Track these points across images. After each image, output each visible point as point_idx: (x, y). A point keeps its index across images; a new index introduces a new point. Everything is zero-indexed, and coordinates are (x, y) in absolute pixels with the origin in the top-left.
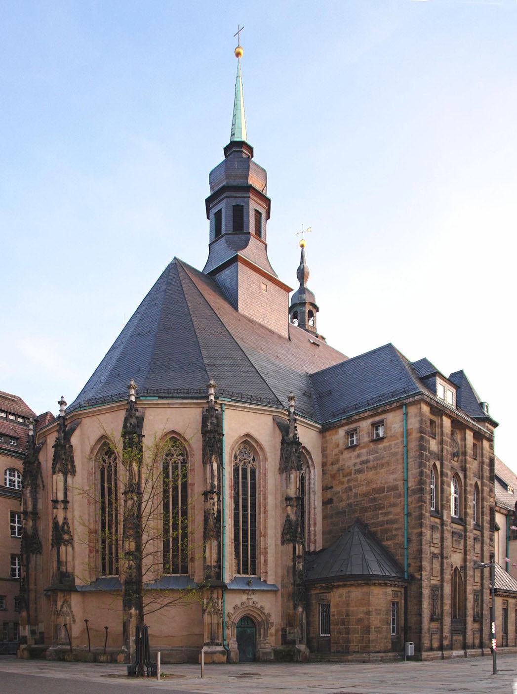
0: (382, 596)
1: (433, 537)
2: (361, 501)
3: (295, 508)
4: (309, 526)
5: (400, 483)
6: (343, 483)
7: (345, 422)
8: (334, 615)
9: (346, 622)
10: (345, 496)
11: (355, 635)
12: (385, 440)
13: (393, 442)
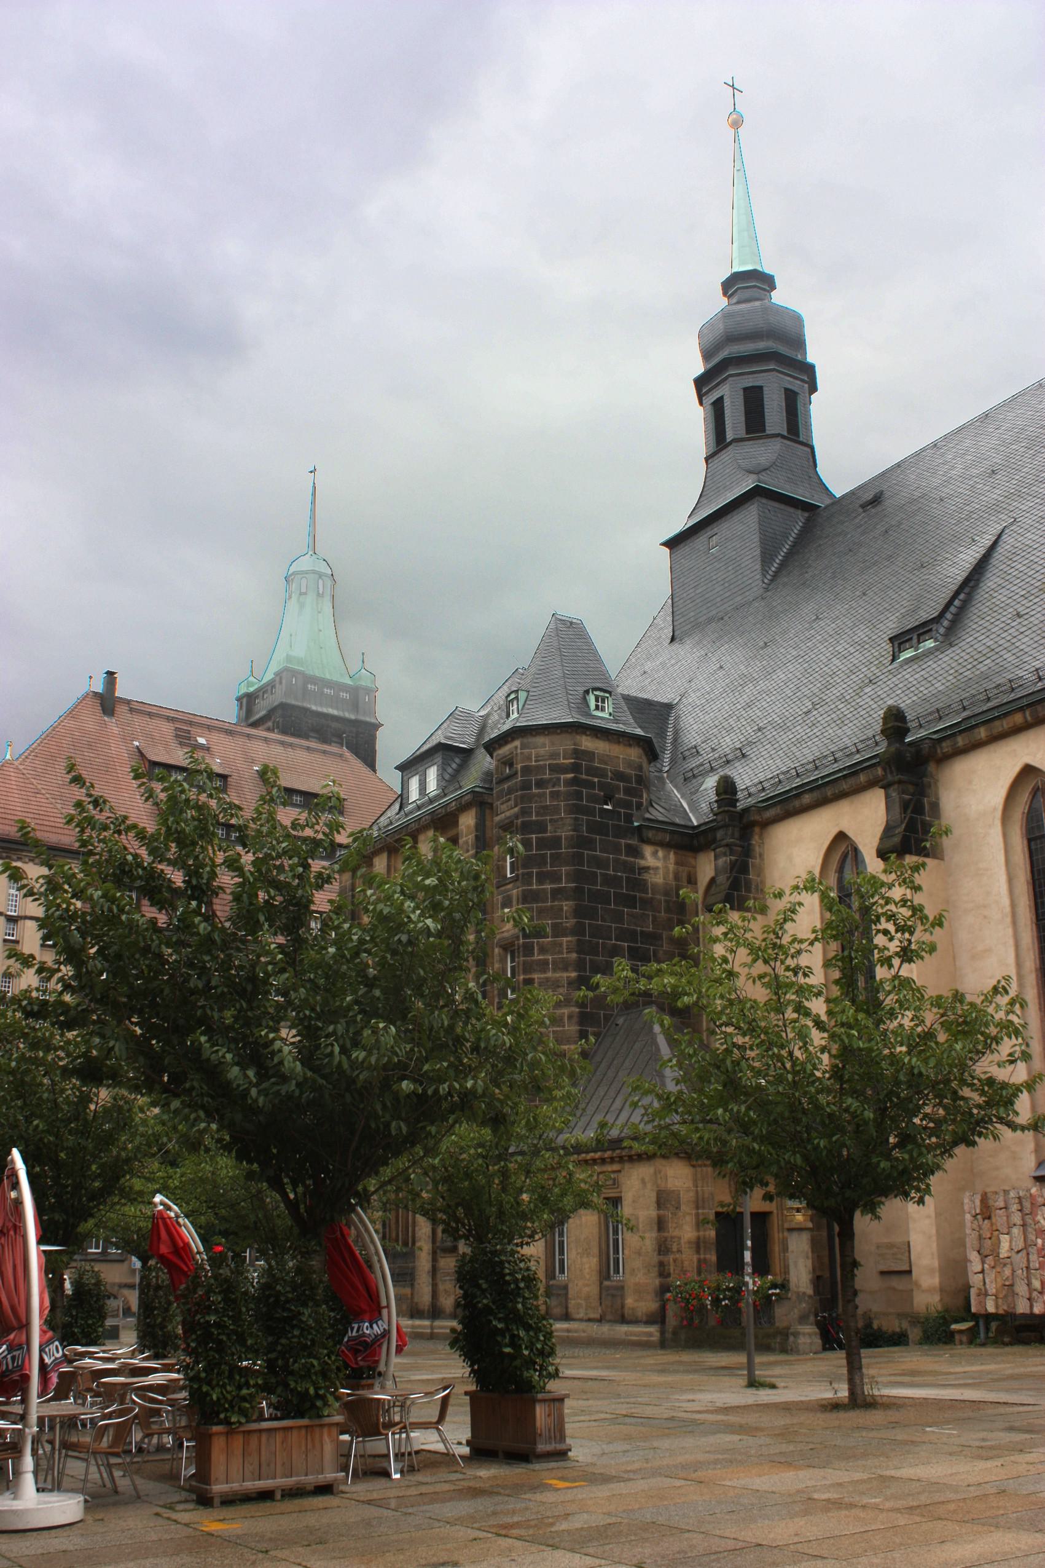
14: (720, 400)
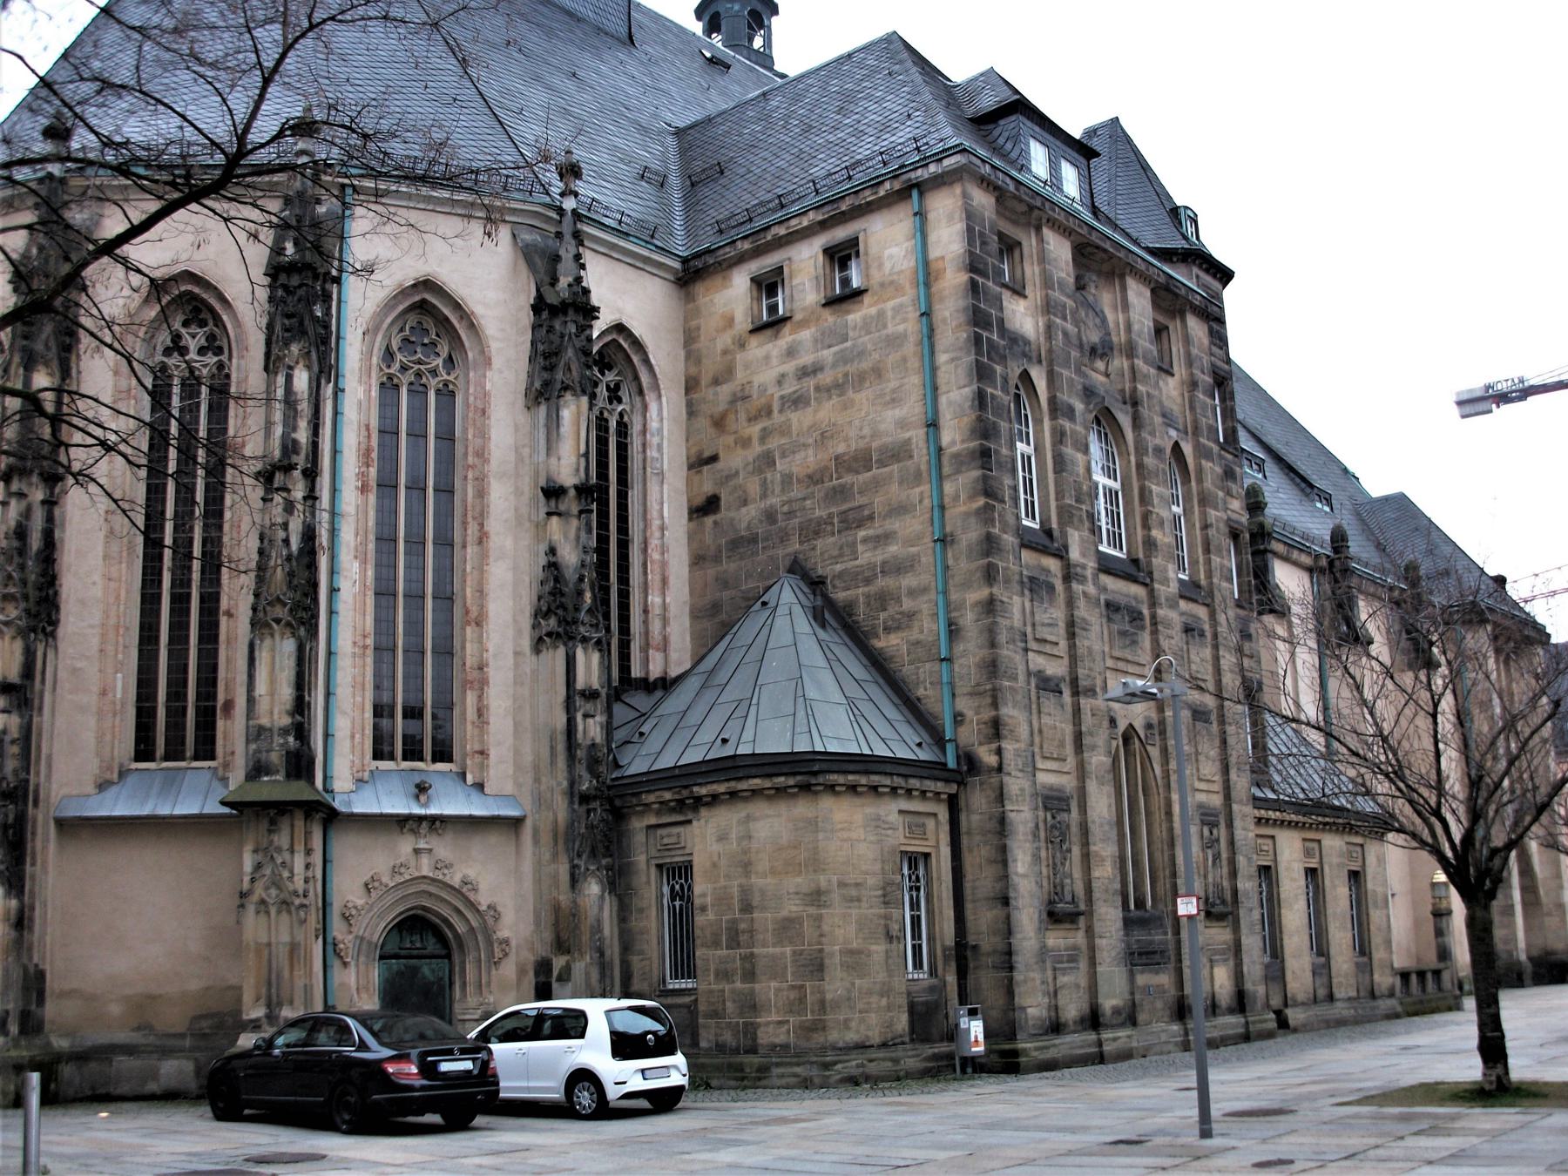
0: (861, 831)
1: (1037, 618)
2: (804, 499)
3: (575, 523)
5: (917, 435)
6: (745, 443)
7: (747, 245)
8: (703, 909)
9: (743, 932)
10: (753, 487)
11: (773, 984)
12: (867, 299)
13: (891, 304)
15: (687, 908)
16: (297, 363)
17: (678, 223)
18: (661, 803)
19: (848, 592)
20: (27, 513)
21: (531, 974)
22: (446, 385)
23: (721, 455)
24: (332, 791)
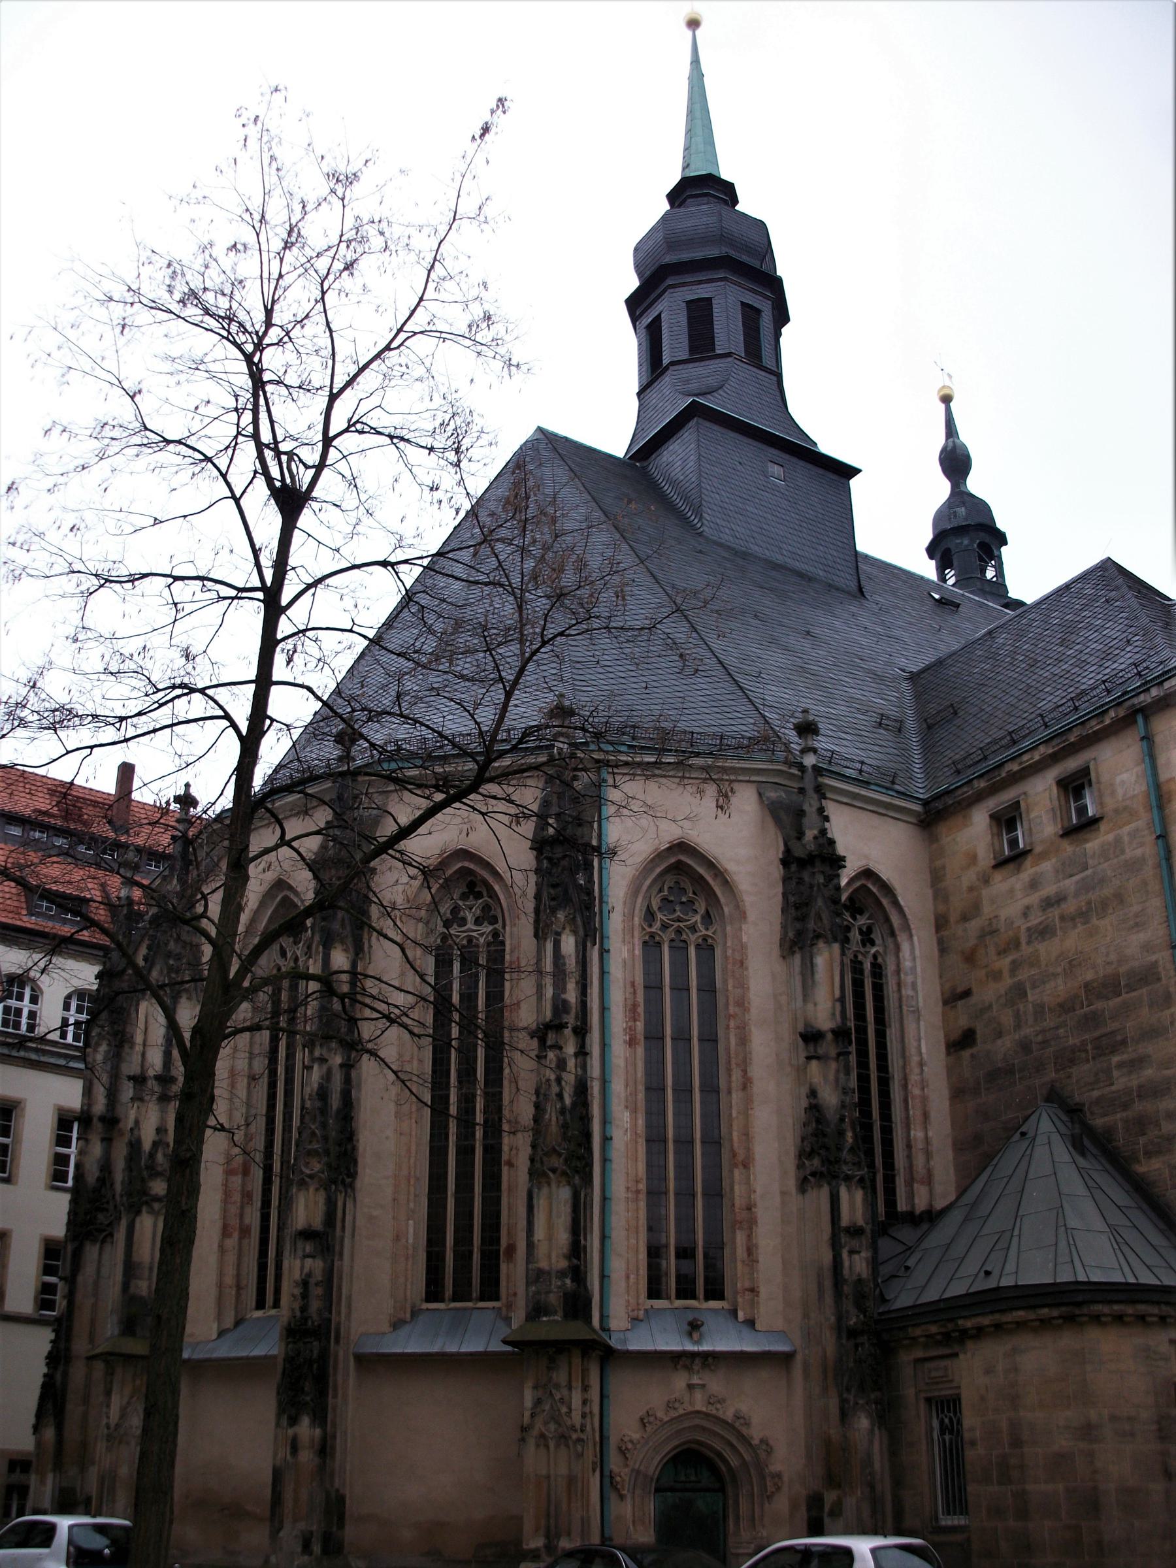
2: (1057, 1028)
3: (833, 1065)
4: (908, 1126)
6: (996, 976)
7: (983, 784)
8: (973, 1443)
10: (1007, 1018)
12: (1103, 826)
14: (657, 322)
15: (957, 1442)
16: (564, 928)
17: (917, 767)
18: (926, 1336)
19: (1106, 1119)
20: (328, 1076)
21: (804, 1508)
22: (705, 940)
23: (974, 990)
24: (609, 1330)
